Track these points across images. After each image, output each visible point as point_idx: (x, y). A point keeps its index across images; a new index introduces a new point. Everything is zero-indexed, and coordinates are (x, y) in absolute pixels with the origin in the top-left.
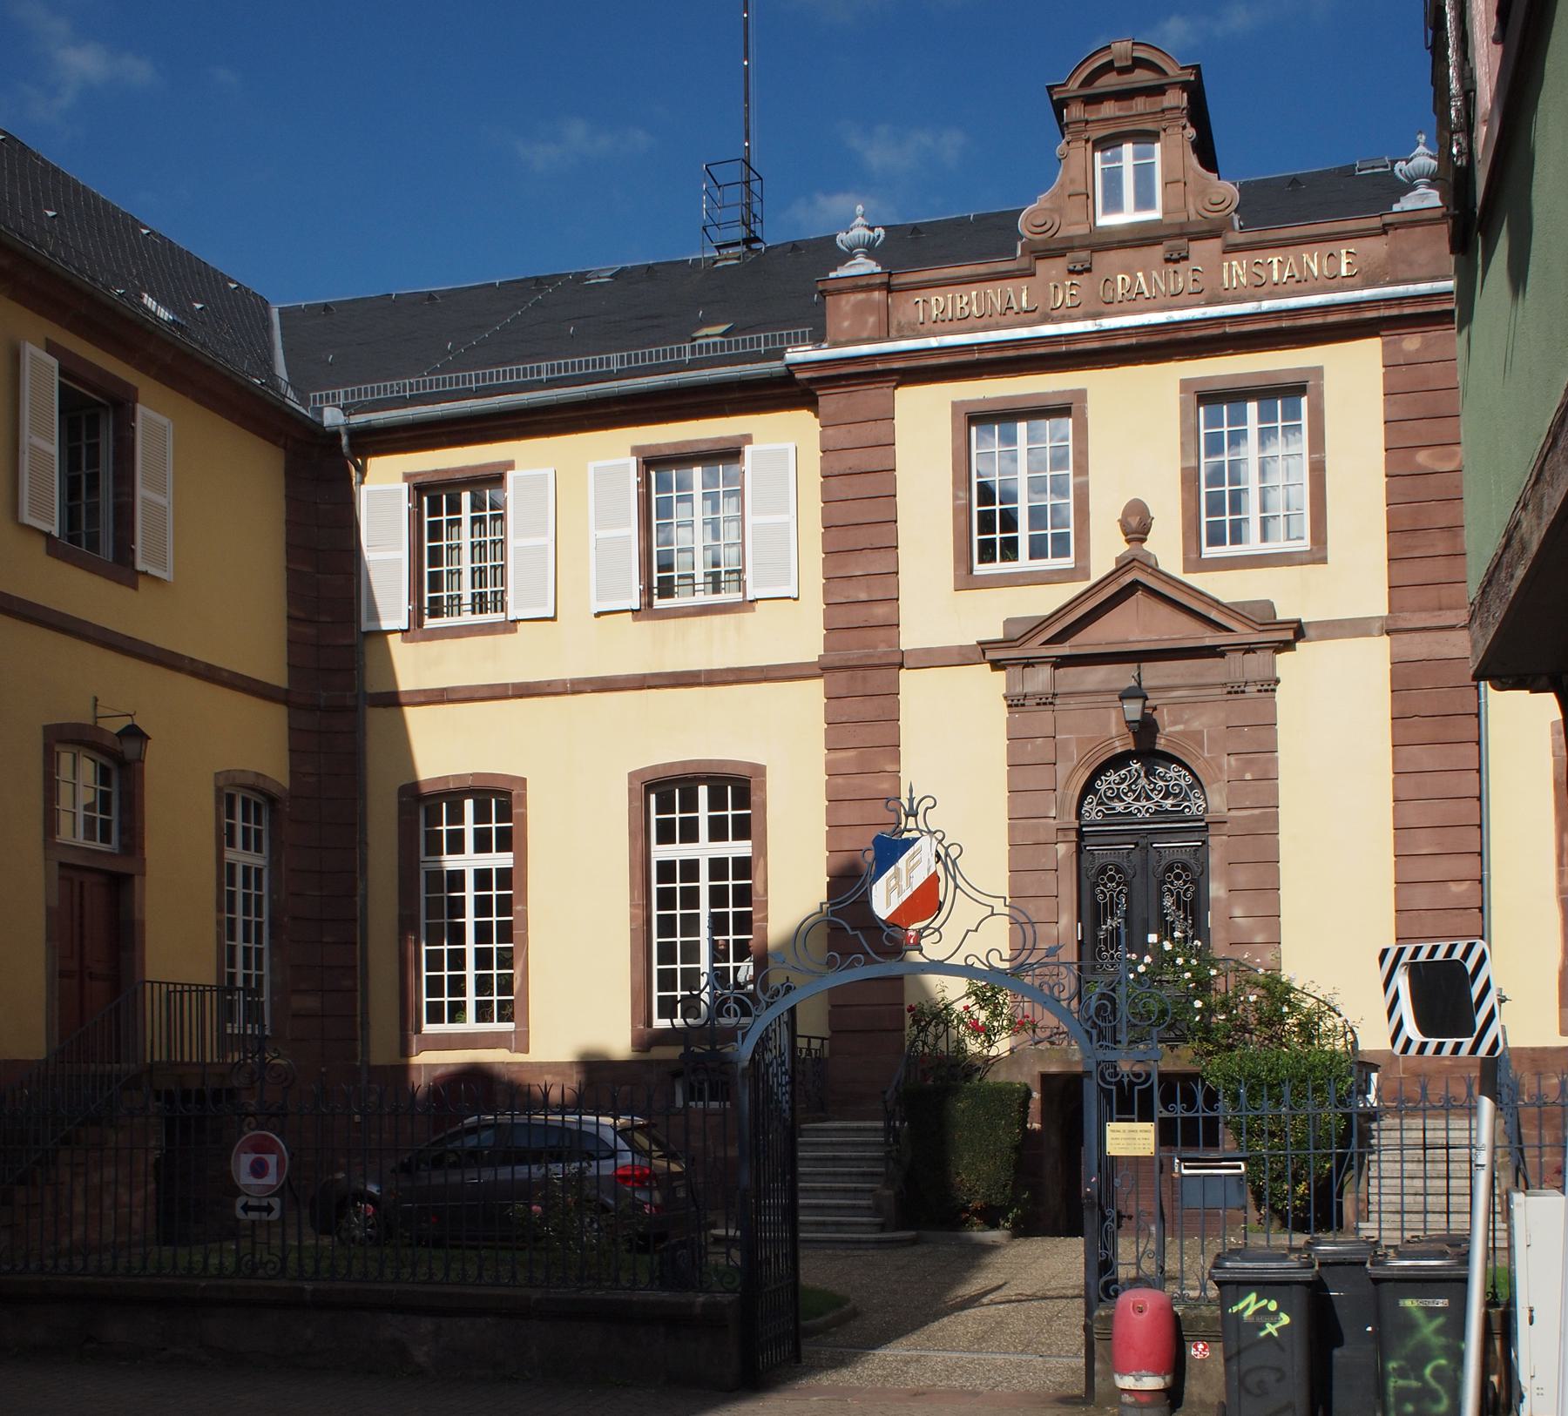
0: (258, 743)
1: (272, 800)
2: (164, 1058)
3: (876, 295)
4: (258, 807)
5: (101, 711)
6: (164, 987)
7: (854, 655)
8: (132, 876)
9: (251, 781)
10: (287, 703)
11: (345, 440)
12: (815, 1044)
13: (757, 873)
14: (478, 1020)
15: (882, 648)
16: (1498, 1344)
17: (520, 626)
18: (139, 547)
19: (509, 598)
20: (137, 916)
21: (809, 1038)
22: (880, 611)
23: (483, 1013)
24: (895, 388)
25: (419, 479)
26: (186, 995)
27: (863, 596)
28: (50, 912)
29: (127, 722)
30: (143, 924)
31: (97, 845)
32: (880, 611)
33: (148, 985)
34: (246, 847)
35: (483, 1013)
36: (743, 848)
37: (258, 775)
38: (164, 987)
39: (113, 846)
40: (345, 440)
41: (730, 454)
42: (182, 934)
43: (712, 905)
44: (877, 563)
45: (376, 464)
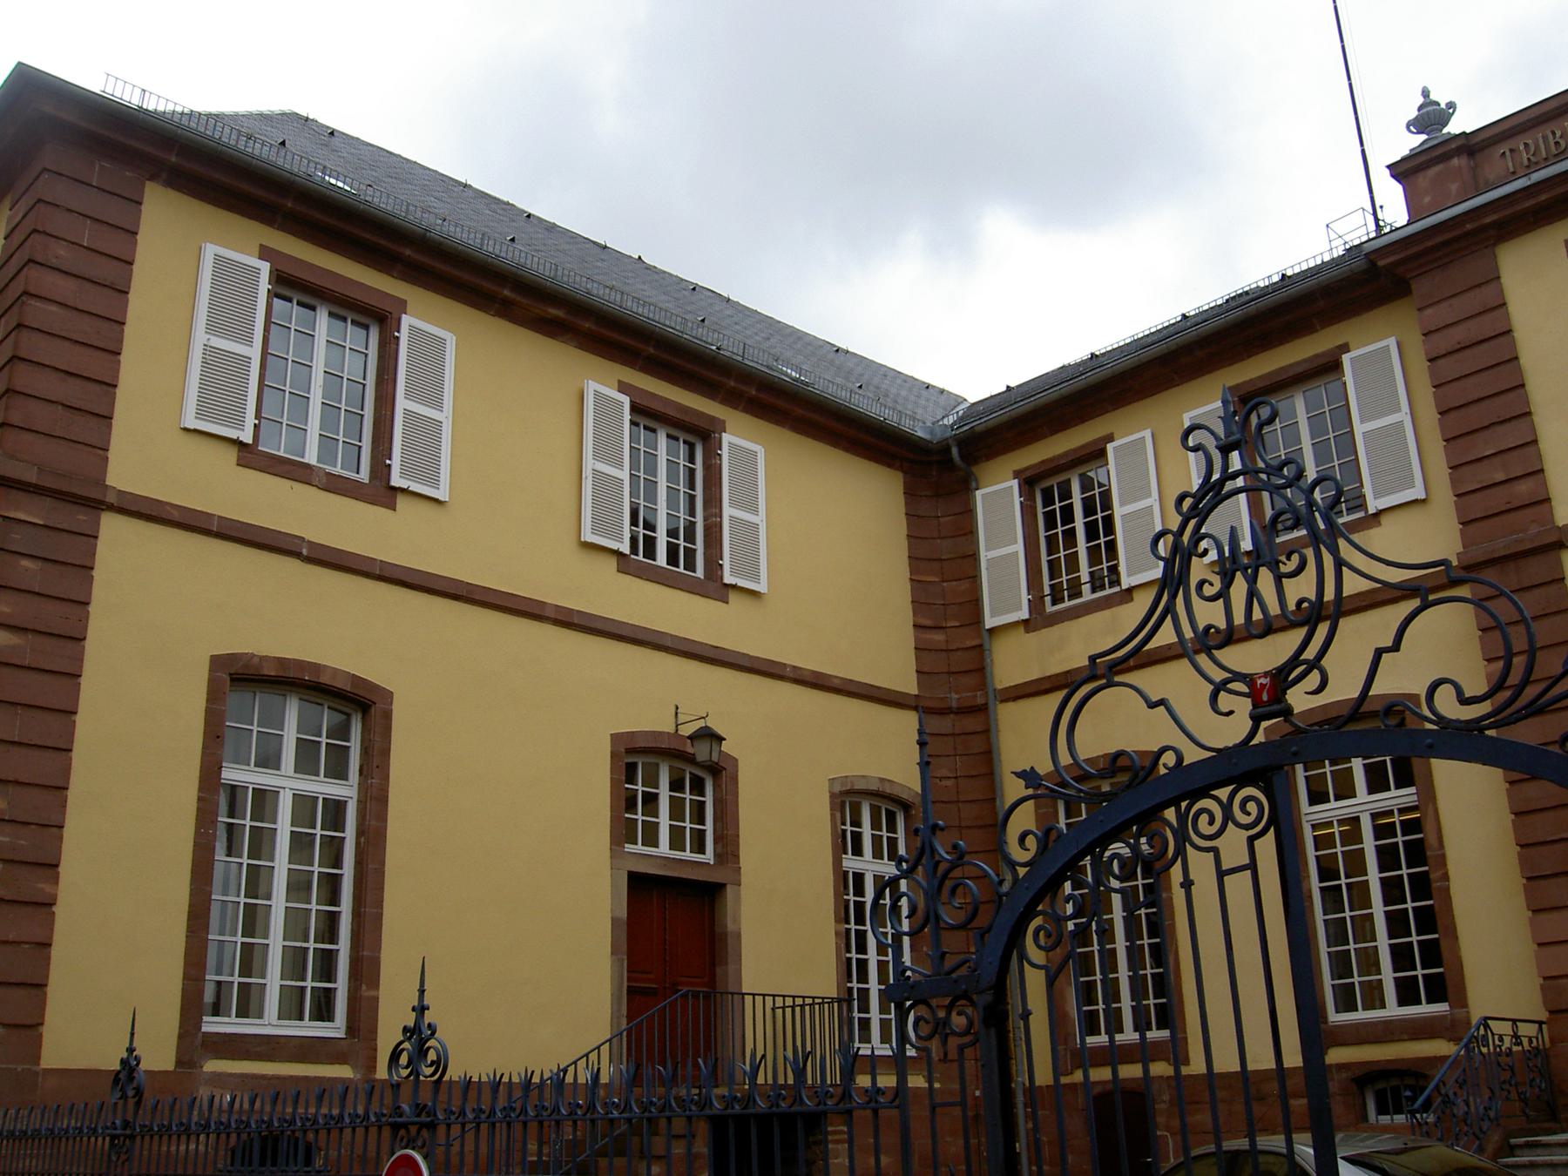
0: (890, 751)
1: (906, 807)
2: (770, 1081)
3: (1455, 161)
4: (891, 817)
5: (682, 719)
6: (769, 1000)
7: (1500, 547)
8: (723, 886)
9: (874, 787)
10: (916, 708)
11: (955, 451)
12: (1526, 1030)
13: (1429, 826)
14: (1402, 1002)
15: (1534, 529)
16: (800, 411)
17: (1384, 519)
18: (726, 563)
19: (1122, 569)
20: (730, 926)
21: (1514, 1021)
22: (1524, 489)
23: (1407, 994)
24: (1495, 245)
25: (1028, 474)
26: (798, 1009)
27: (1500, 477)
28: (614, 921)
29: (701, 723)
30: (738, 936)
31: (687, 855)
32: (1524, 489)
33: (748, 999)
34: (877, 854)
35: (1407, 994)
36: (1407, 795)
37: (882, 780)
38: (769, 1000)
39: (709, 856)
40: (955, 451)
41: (1330, 366)
42: (785, 944)
43: (1382, 869)
44: (1508, 436)
45: (984, 470)
